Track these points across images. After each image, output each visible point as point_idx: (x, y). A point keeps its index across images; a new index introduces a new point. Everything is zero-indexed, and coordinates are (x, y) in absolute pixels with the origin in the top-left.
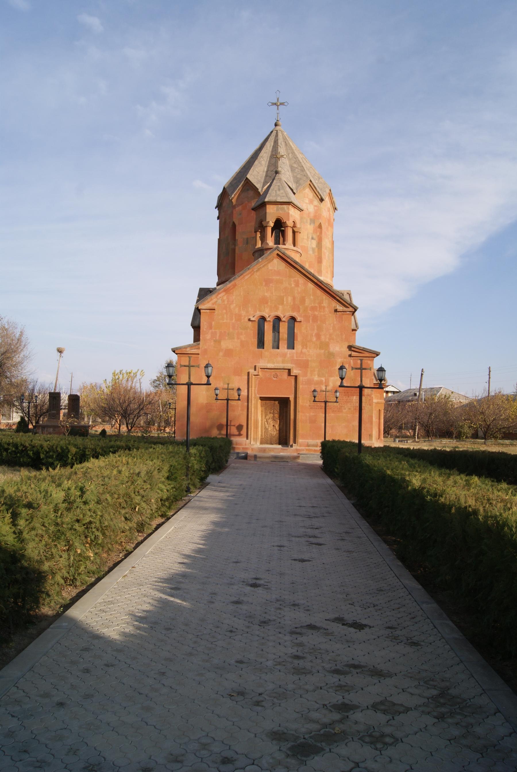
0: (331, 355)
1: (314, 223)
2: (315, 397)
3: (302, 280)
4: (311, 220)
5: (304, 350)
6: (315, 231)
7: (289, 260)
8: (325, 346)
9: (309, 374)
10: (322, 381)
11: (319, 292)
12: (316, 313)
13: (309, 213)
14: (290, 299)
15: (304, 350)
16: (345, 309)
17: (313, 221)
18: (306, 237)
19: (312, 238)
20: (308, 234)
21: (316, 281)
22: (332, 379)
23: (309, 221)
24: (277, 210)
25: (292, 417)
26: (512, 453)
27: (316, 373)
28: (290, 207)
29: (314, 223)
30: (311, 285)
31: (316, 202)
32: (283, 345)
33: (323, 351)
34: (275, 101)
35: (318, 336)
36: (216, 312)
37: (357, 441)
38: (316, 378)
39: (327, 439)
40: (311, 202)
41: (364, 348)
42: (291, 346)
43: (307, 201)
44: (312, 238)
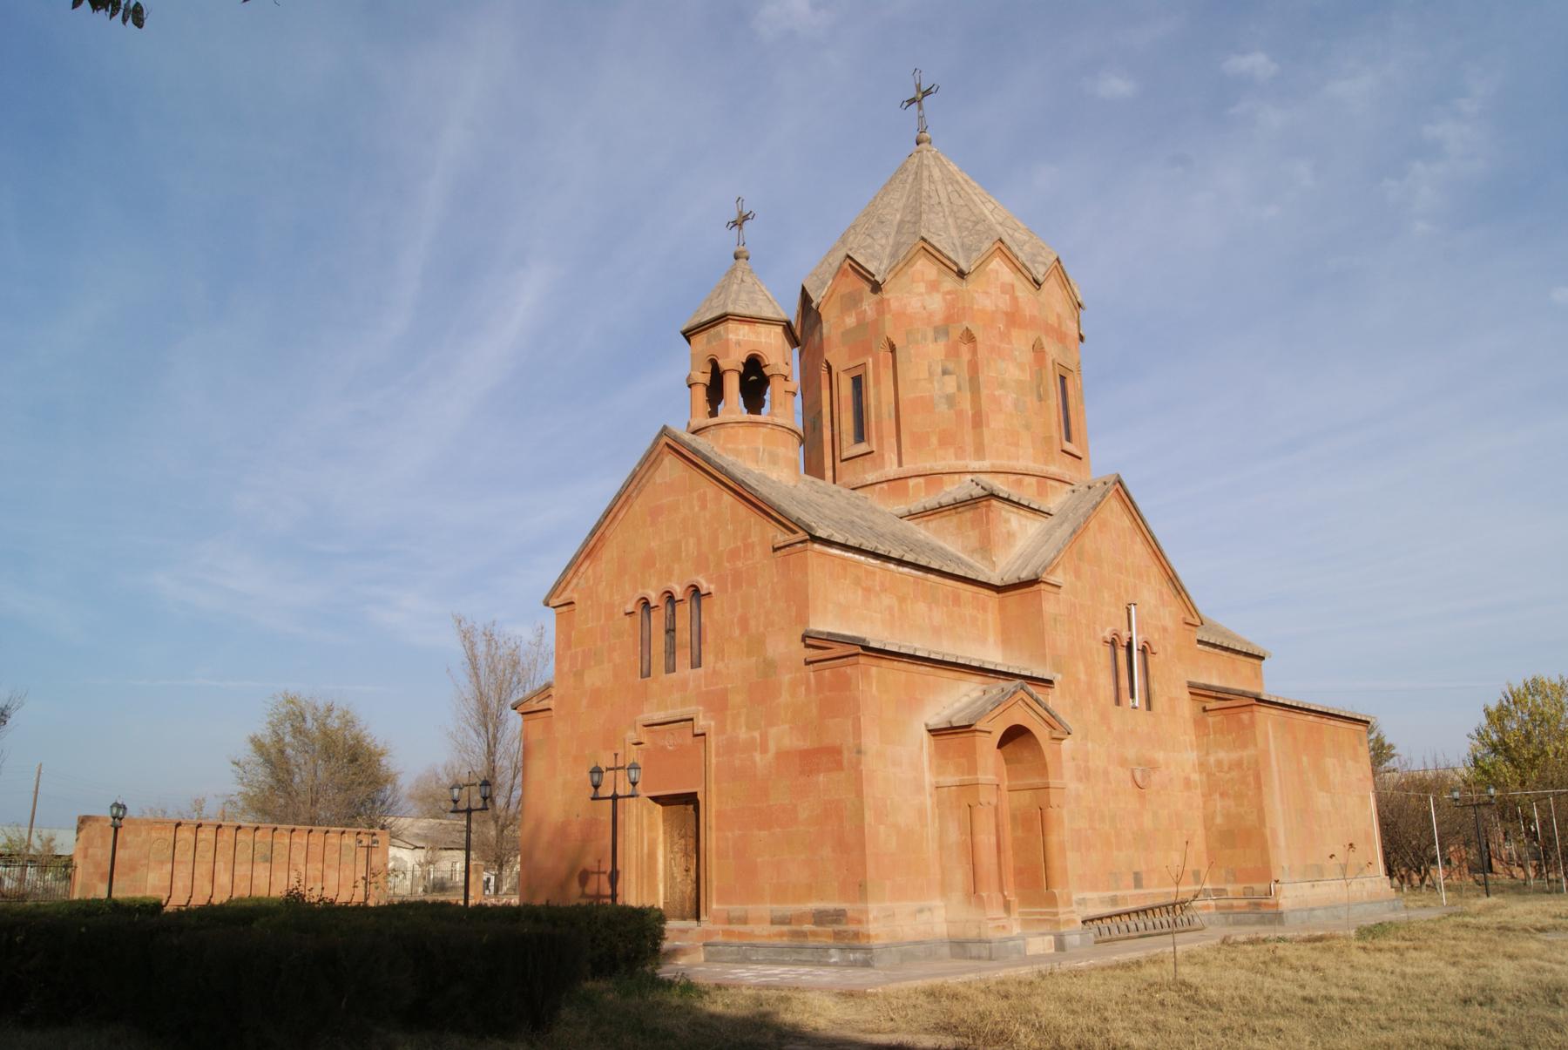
0: (769, 667)
1: (947, 333)
2: (596, 787)
3: (709, 489)
4: (936, 330)
5: (720, 665)
6: (953, 352)
7: (685, 452)
8: (756, 645)
9: (729, 727)
10: (753, 739)
11: (743, 509)
12: (739, 564)
13: (931, 315)
14: (692, 541)
15: (720, 665)
16: (792, 538)
17: (942, 331)
18: (924, 375)
19: (945, 372)
20: (930, 367)
21: (731, 484)
22: (773, 731)
23: (930, 334)
24: (709, 342)
25: (1009, 854)
26: (178, 900)
27: (743, 719)
28: (731, 325)
29: (947, 333)
30: (728, 498)
31: (950, 282)
32: (683, 658)
33: (754, 659)
34: (912, 94)
35: (744, 623)
36: (577, 607)
37: (461, 903)
38: (743, 734)
39: (114, 895)
40: (933, 286)
41: (829, 634)
42: (696, 663)
43: (922, 288)
44: (945, 372)
